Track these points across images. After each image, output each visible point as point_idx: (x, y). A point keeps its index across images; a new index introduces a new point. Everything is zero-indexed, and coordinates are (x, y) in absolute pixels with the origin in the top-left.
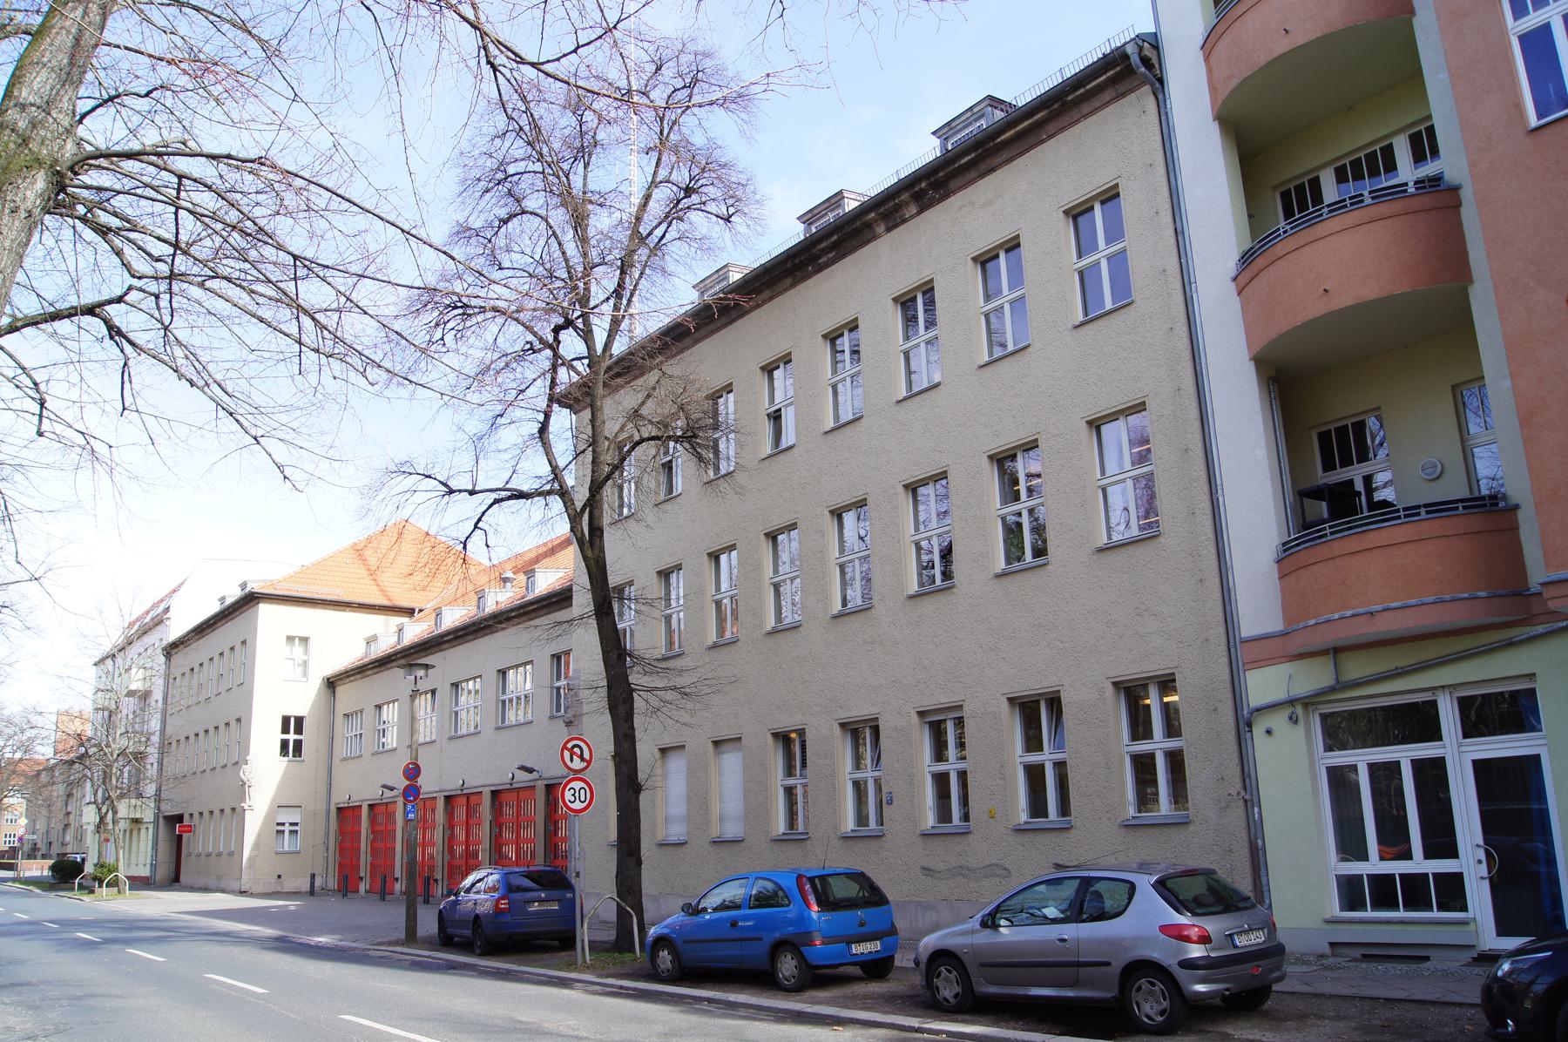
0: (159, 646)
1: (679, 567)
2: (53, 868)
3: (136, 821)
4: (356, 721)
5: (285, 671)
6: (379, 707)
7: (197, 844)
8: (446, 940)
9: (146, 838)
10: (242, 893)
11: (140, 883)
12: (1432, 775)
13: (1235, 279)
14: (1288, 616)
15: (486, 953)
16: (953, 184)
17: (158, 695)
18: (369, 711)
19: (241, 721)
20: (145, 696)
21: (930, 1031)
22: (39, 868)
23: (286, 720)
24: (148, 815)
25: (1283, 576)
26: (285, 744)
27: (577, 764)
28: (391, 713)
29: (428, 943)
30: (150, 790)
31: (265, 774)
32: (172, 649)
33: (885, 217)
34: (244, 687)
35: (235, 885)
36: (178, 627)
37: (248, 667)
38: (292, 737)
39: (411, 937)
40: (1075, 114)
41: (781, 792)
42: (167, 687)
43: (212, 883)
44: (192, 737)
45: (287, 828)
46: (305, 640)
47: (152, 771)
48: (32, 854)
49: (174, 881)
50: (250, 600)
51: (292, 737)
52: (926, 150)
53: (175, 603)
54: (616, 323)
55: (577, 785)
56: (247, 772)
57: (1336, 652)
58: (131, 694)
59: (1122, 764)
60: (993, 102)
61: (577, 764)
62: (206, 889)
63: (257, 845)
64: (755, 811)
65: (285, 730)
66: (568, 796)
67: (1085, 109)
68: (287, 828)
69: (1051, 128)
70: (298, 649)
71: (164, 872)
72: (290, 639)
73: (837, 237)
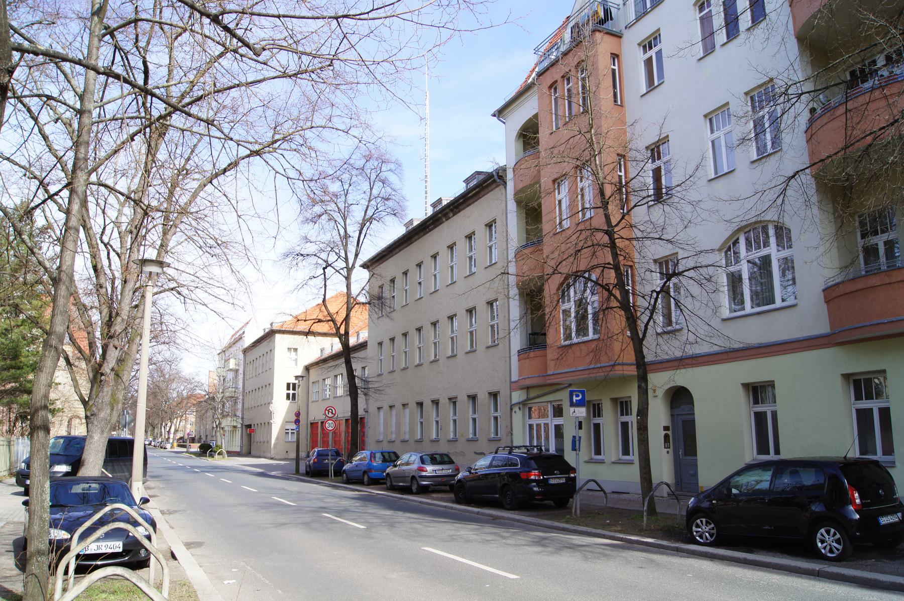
0: (242, 349)
1: (455, 315)
2: (200, 447)
3: (235, 427)
4: (317, 385)
5: (290, 361)
6: (324, 380)
7: (258, 436)
8: (308, 474)
9: (238, 433)
10: (272, 459)
11: (231, 454)
12: (546, 425)
13: (806, 132)
14: (832, 323)
15: (312, 477)
16: (461, 207)
17: (241, 371)
18: (321, 381)
19: (270, 385)
20: (236, 371)
21: (456, 509)
22: (195, 448)
23: (288, 385)
24: (239, 426)
25: (827, 302)
26: (288, 395)
27: (330, 415)
28: (328, 382)
29: (303, 475)
30: (239, 414)
31: (280, 409)
32: (245, 351)
33: (452, 210)
34: (270, 370)
35: (269, 455)
36: (248, 341)
37: (272, 360)
38: (291, 392)
39: (297, 471)
40: (487, 190)
41: (452, 422)
42: (244, 367)
43: (262, 454)
44: (387, 342)
45: (290, 431)
46: (296, 350)
47: (240, 406)
48: (193, 440)
49: (248, 454)
50: (270, 335)
51: (291, 392)
52: (460, 189)
53: (246, 329)
54: (357, 255)
55: (330, 422)
56: (273, 407)
57: (528, 388)
58: (231, 370)
59: (490, 419)
60: (478, 173)
61: (330, 415)
62: (260, 457)
63: (277, 439)
64: (412, 431)
65: (288, 388)
66: (327, 425)
67: (490, 189)
68: (290, 431)
69: (482, 193)
70: (293, 353)
71: (245, 450)
72: (289, 349)
73: (443, 214)
